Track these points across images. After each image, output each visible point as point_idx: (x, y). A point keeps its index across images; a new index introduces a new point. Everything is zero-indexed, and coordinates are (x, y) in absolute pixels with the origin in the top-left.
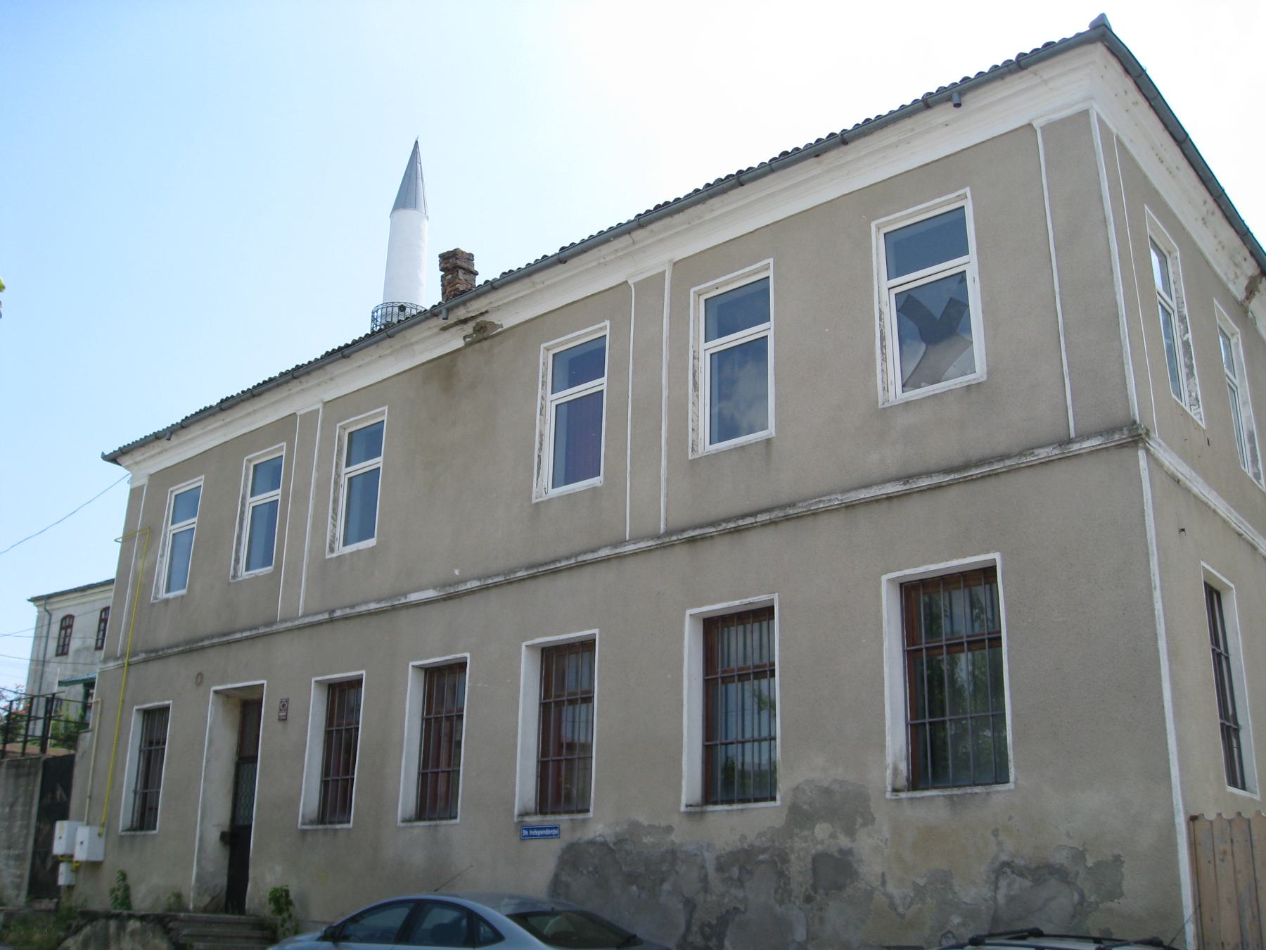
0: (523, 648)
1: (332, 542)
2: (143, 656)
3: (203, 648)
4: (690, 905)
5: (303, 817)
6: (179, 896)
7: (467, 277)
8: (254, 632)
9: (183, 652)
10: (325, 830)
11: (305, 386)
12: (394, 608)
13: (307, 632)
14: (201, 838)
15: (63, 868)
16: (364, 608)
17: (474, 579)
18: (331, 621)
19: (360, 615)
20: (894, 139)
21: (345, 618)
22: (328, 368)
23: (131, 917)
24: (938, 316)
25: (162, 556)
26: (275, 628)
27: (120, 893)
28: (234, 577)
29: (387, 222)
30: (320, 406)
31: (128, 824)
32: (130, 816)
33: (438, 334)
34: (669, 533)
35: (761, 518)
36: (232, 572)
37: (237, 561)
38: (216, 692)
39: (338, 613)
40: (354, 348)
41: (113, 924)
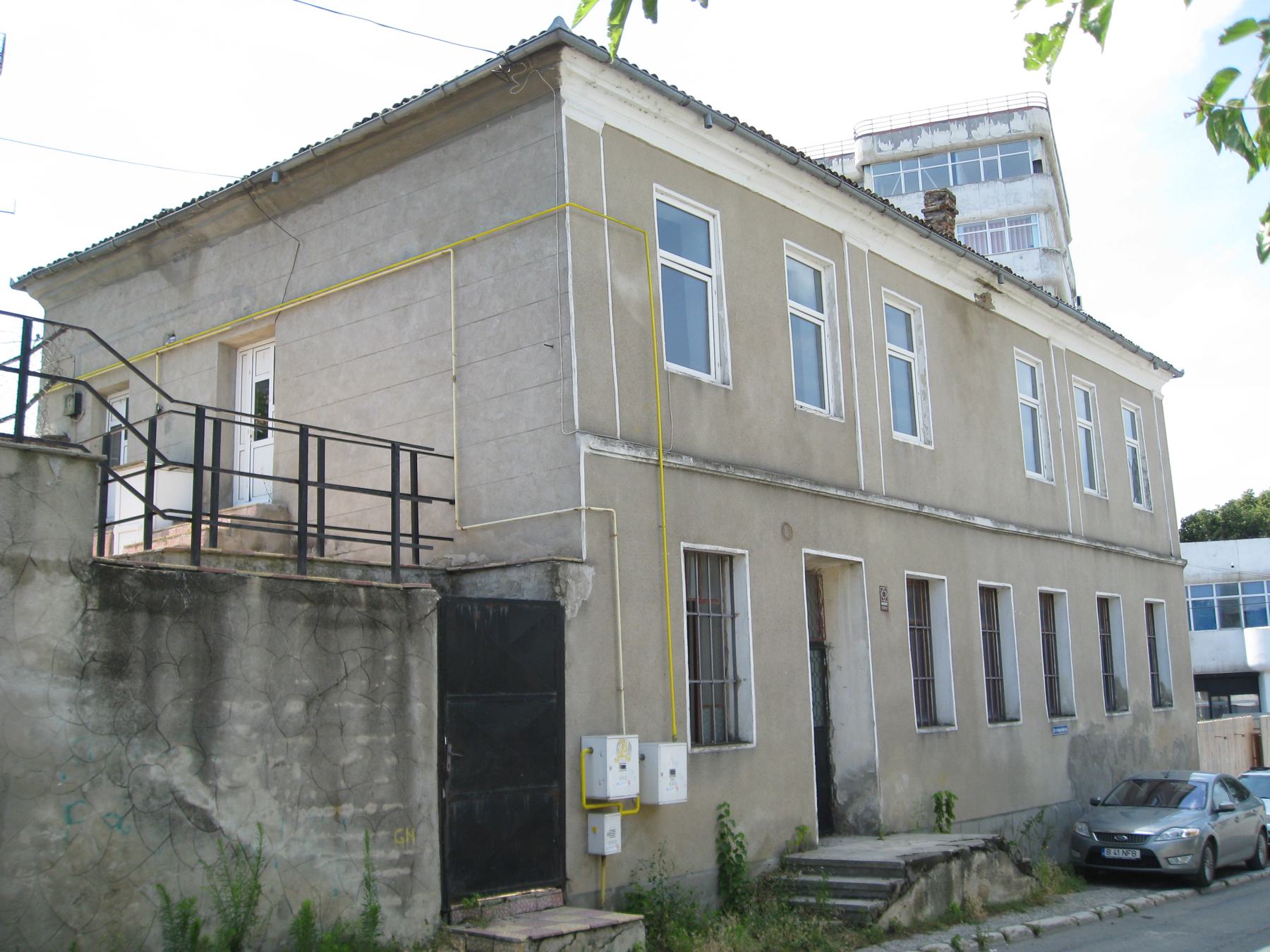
3: (786, 488)
4: (1112, 770)
6: (801, 829)
8: (850, 495)
9: (757, 483)
10: (939, 733)
11: (868, 219)
12: (963, 525)
13: (893, 515)
16: (944, 514)
17: (992, 519)
18: (917, 514)
20: (646, 104)
21: (927, 516)
22: (901, 226)
26: (870, 499)
33: (970, 278)
35: (794, 484)
39: (926, 510)
40: (764, 142)
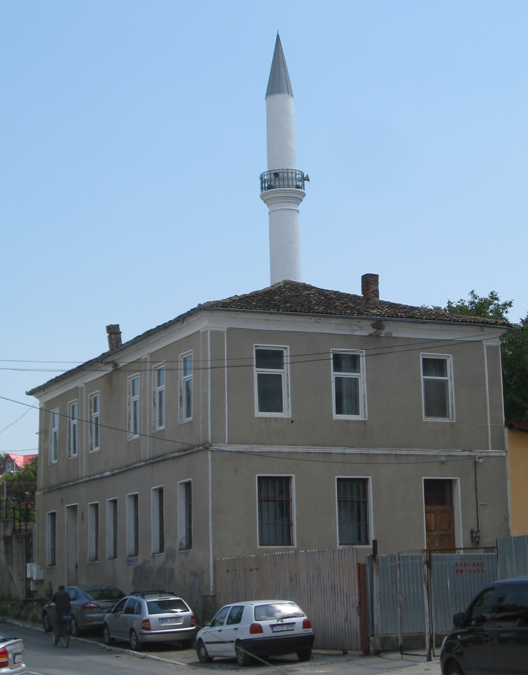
0: (127, 498)
1: (91, 446)
2: (47, 490)
5: (89, 558)
7: (116, 336)
14: (68, 568)
15: (32, 583)
19: (94, 480)
23: (34, 601)
24: (359, 293)
25: (51, 443)
27: (48, 592)
28: (69, 456)
29: (264, 102)
30: (83, 385)
31: (50, 563)
32: (50, 560)
34: (150, 459)
36: (68, 455)
37: (70, 449)
38: (68, 507)
41: (31, 604)
